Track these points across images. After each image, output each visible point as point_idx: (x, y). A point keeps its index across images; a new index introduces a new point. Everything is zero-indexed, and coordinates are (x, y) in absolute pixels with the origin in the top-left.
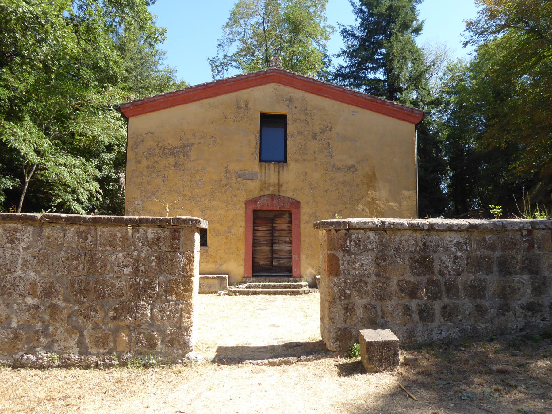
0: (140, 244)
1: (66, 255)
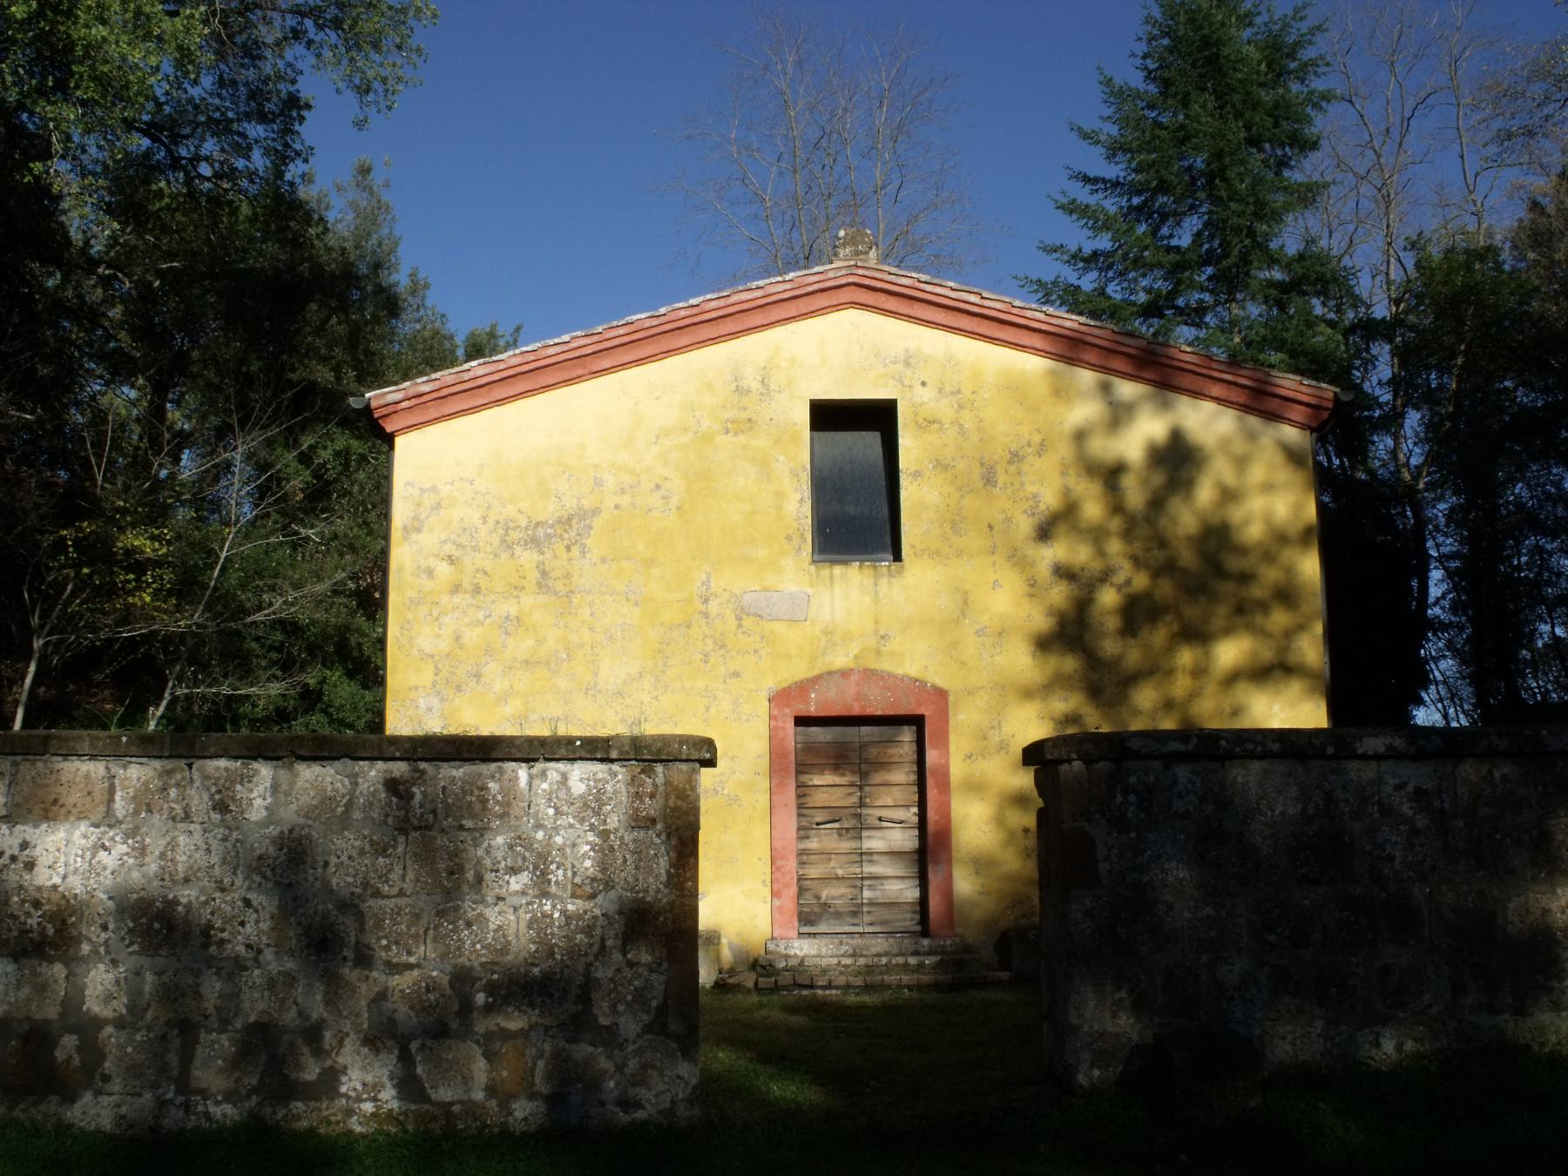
0: (551, 811)
1: (357, 843)
